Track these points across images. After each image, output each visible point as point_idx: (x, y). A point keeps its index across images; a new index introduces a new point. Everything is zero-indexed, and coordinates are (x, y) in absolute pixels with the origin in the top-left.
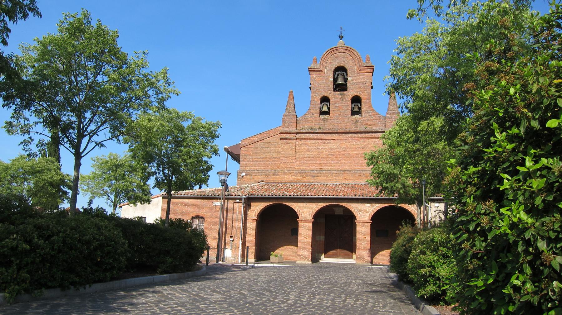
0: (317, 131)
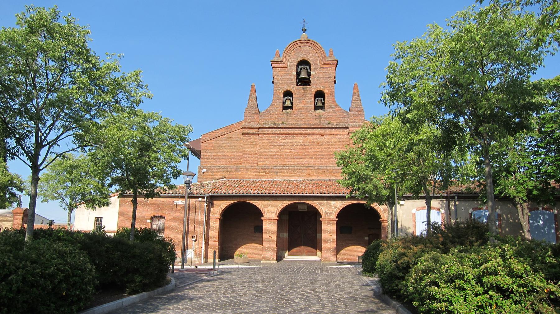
0: (280, 126)
